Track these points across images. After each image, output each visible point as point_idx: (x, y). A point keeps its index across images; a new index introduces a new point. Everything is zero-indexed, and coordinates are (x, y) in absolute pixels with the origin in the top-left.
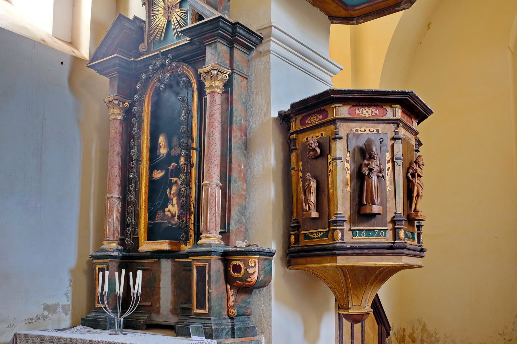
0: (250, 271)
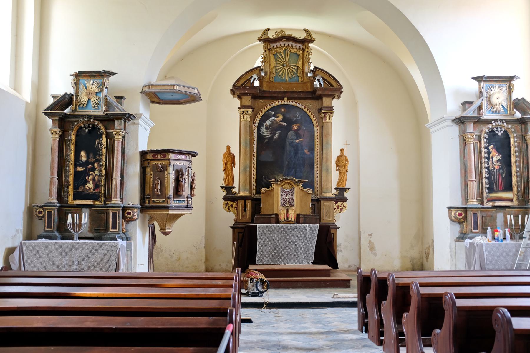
0: (135, 214)
